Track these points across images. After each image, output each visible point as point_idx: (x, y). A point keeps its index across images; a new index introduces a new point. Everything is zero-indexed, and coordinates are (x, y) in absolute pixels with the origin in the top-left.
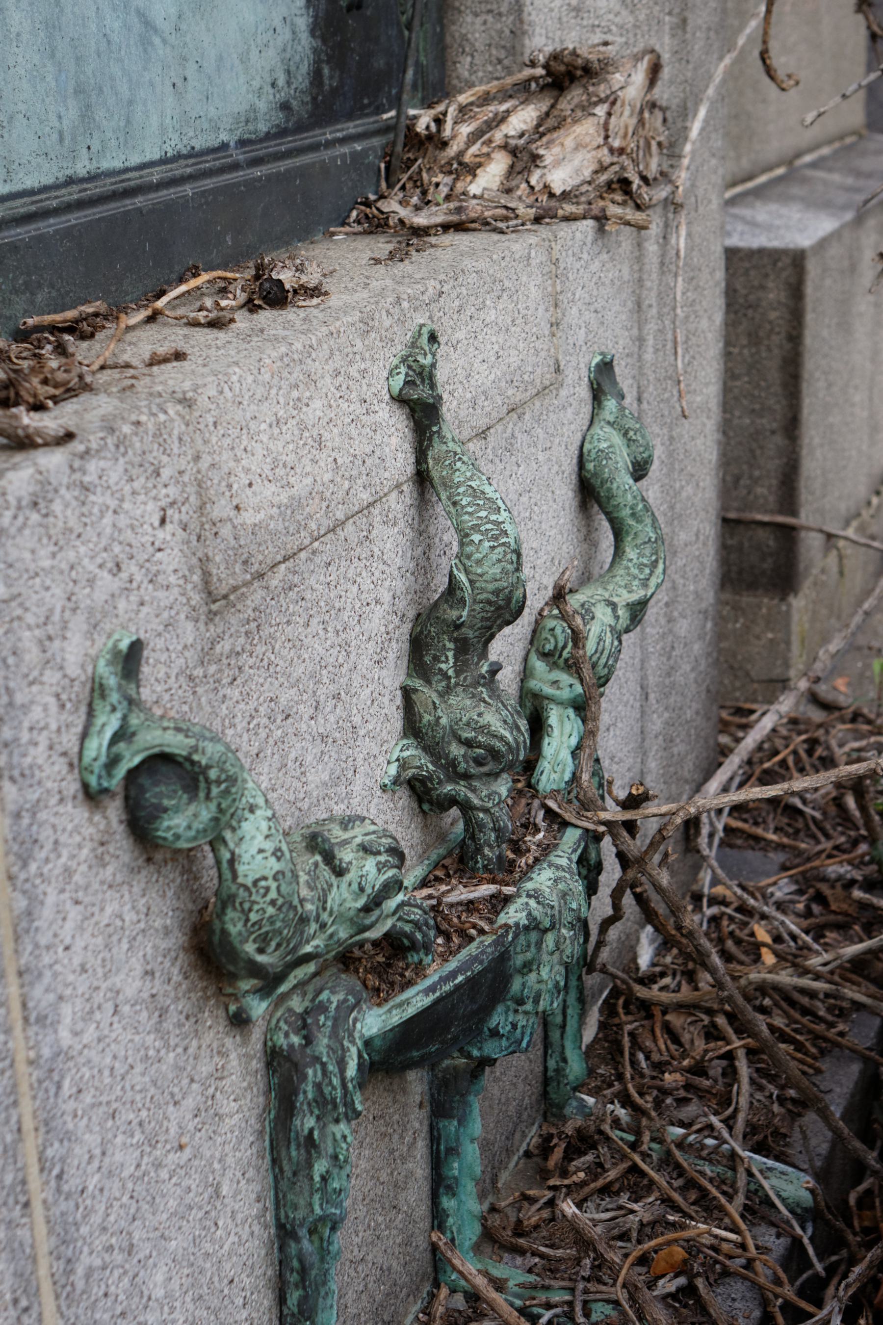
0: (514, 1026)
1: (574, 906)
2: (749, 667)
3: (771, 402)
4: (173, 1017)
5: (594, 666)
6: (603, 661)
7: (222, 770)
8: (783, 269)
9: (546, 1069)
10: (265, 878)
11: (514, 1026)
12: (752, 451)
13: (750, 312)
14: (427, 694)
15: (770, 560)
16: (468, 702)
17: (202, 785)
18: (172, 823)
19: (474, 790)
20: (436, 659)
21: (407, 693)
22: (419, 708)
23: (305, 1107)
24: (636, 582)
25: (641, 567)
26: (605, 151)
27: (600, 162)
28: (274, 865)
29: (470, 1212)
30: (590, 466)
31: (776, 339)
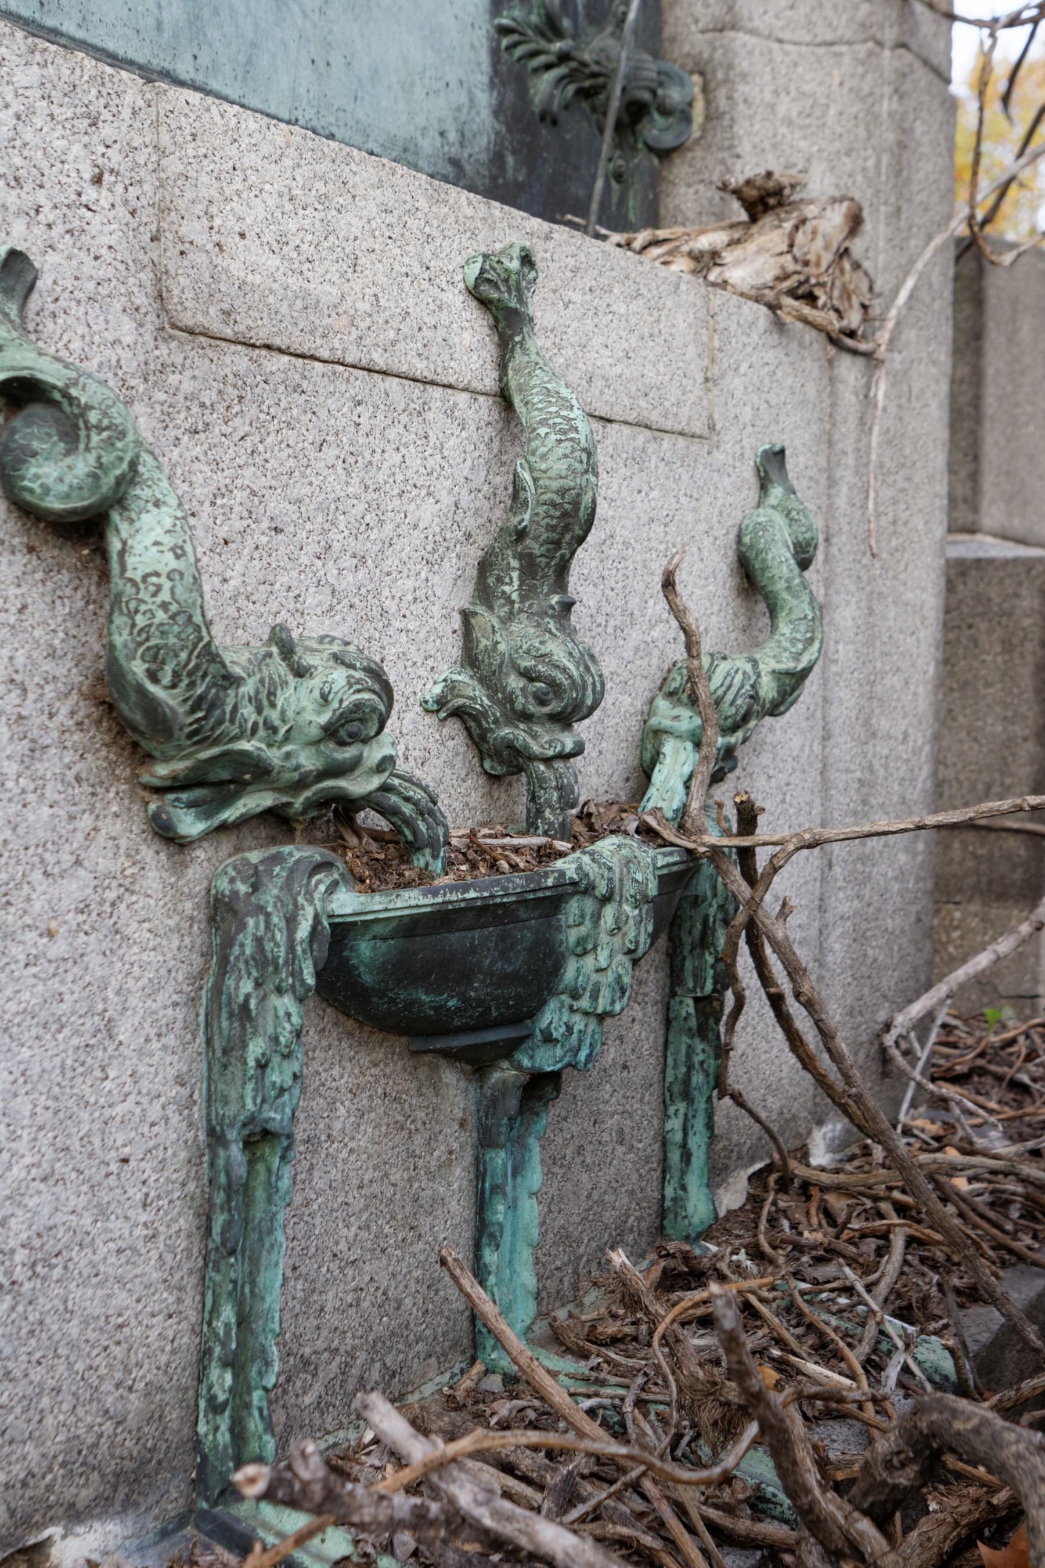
0: (569, 1029)
1: (639, 877)
2: (997, 981)
3: (1024, 708)
4: (51, 764)
5: (718, 702)
6: (729, 697)
7: (105, 414)
8: (1037, 577)
9: (663, 1197)
10: (157, 574)
11: (569, 1029)
12: (1004, 759)
13: (1004, 620)
14: (486, 619)
15: (1020, 870)
16: (532, 630)
17: (83, 433)
18: (40, 471)
19: (535, 737)
20: (500, 580)
21: (466, 616)
22: (477, 633)
23: (242, 965)
24: (787, 654)
25: (793, 641)
26: (789, 257)
27: (783, 268)
28: (169, 561)
29: (524, 1286)
30: (747, 540)
31: (1029, 646)
